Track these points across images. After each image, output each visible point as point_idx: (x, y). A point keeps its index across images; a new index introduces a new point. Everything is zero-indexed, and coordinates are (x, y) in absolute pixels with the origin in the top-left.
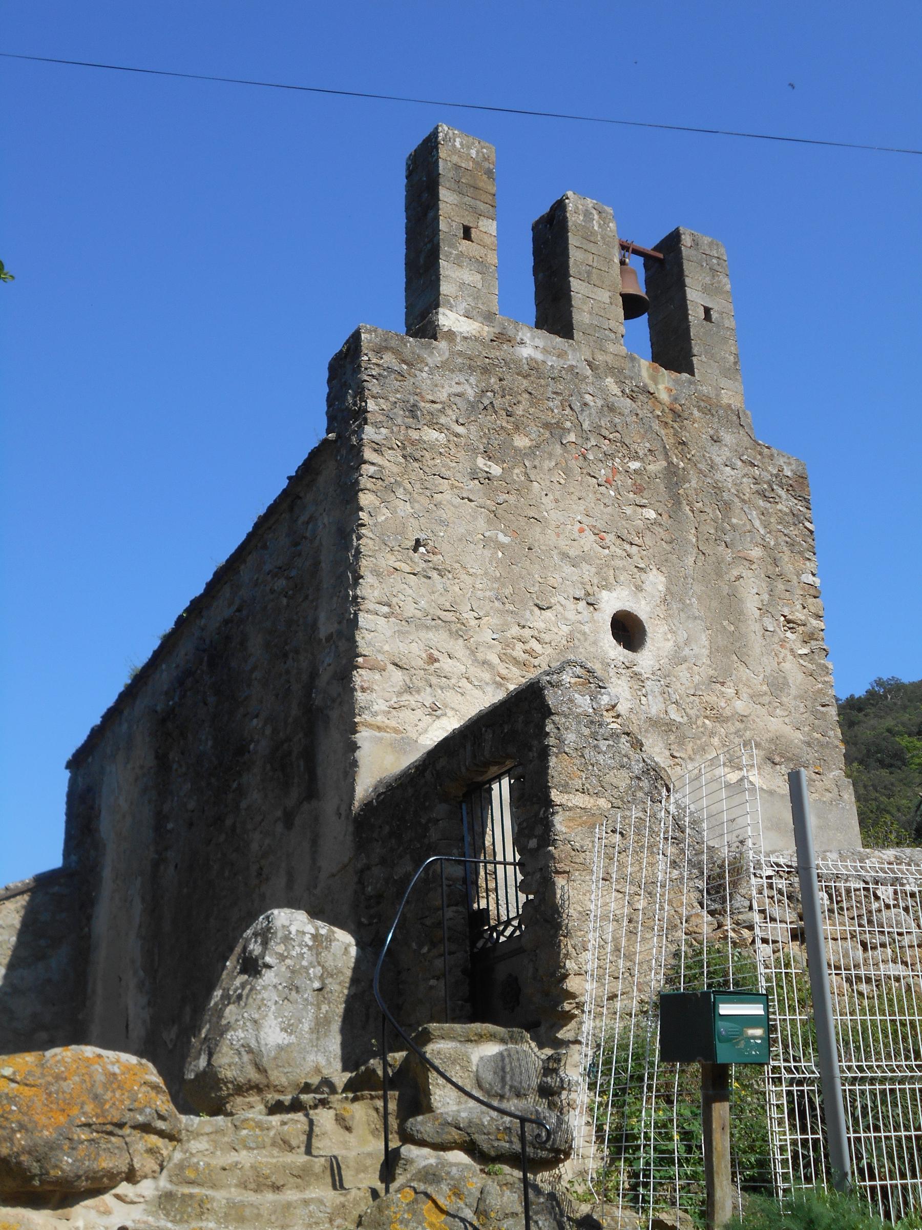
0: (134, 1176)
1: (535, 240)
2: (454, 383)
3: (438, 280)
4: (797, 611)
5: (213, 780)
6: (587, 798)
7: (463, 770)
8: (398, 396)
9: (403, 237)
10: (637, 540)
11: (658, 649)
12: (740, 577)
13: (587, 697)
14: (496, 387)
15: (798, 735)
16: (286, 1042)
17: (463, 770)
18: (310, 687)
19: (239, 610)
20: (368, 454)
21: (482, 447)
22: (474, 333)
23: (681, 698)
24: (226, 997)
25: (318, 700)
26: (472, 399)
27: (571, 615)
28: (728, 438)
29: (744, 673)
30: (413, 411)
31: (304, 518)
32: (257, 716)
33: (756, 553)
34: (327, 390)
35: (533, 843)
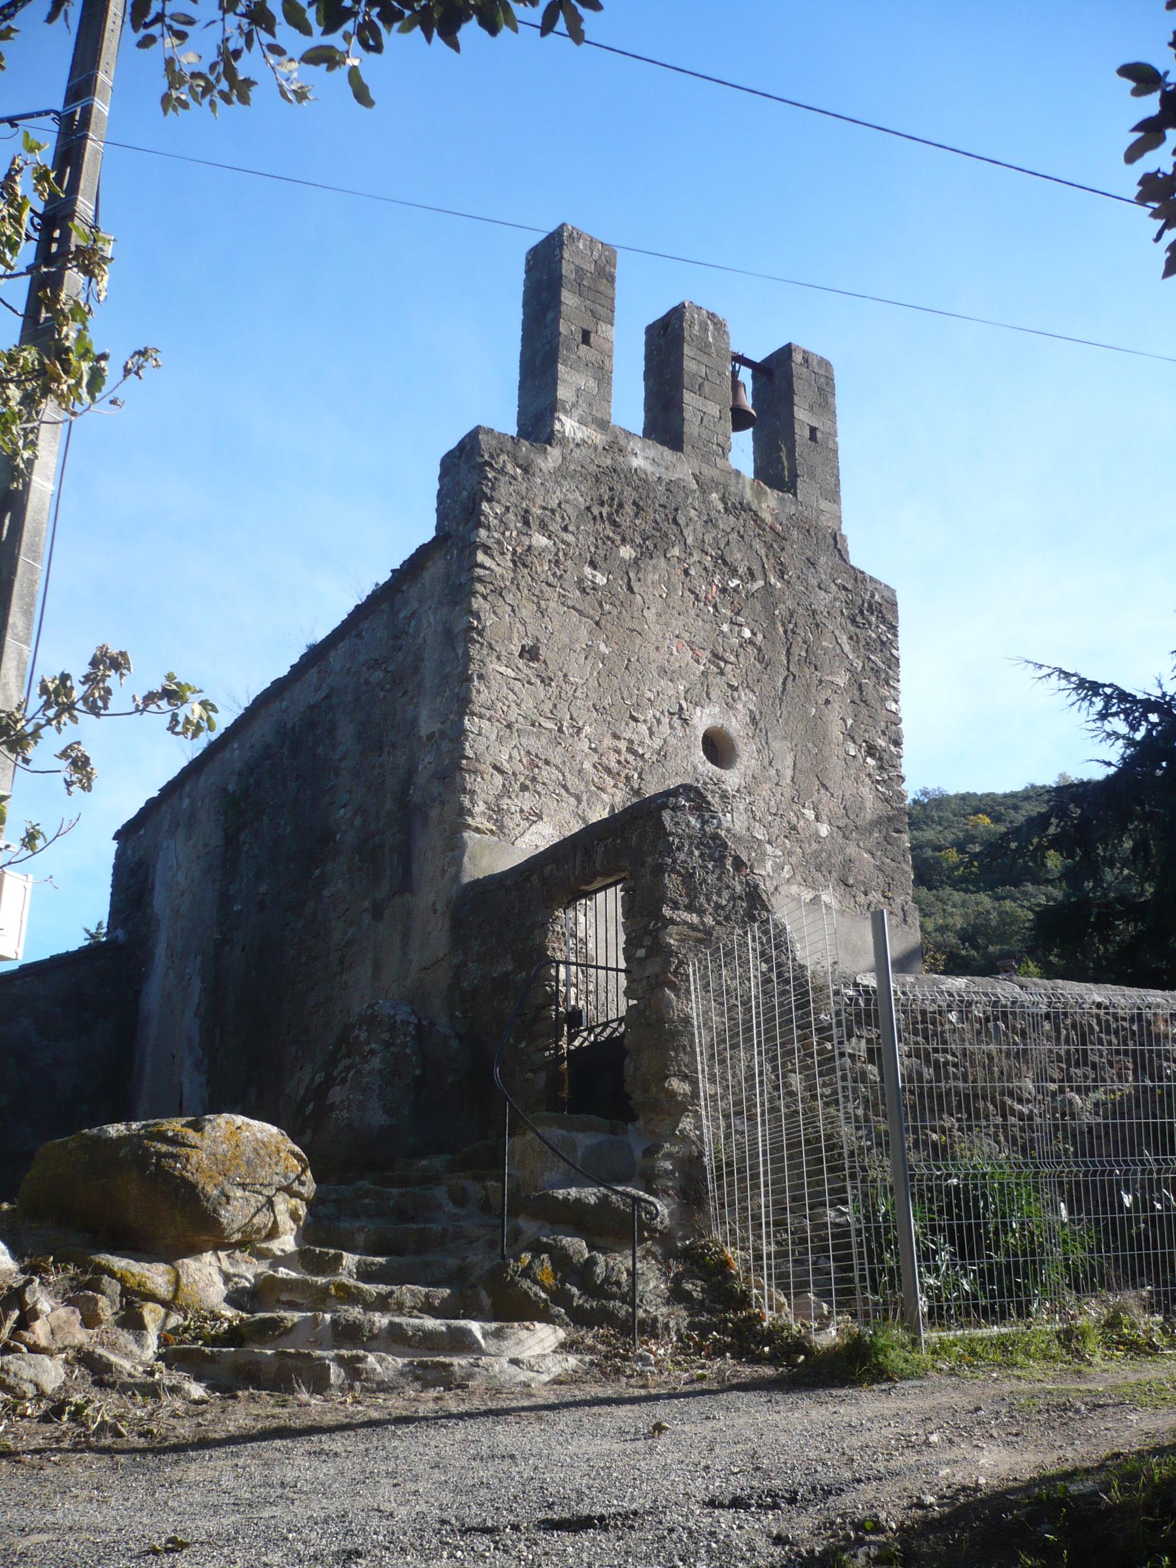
9: (519, 333)
10: (732, 659)
17: (572, 878)
19: (328, 697)
25: (416, 796)
31: (404, 613)
32: (344, 806)
34: (438, 487)
35: (641, 953)
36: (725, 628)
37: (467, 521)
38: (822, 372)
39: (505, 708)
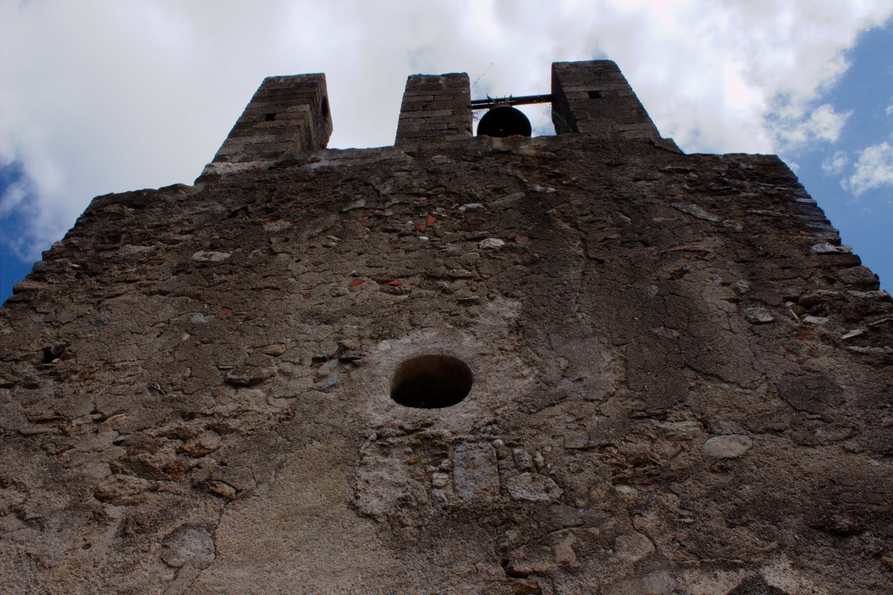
12: (681, 273)
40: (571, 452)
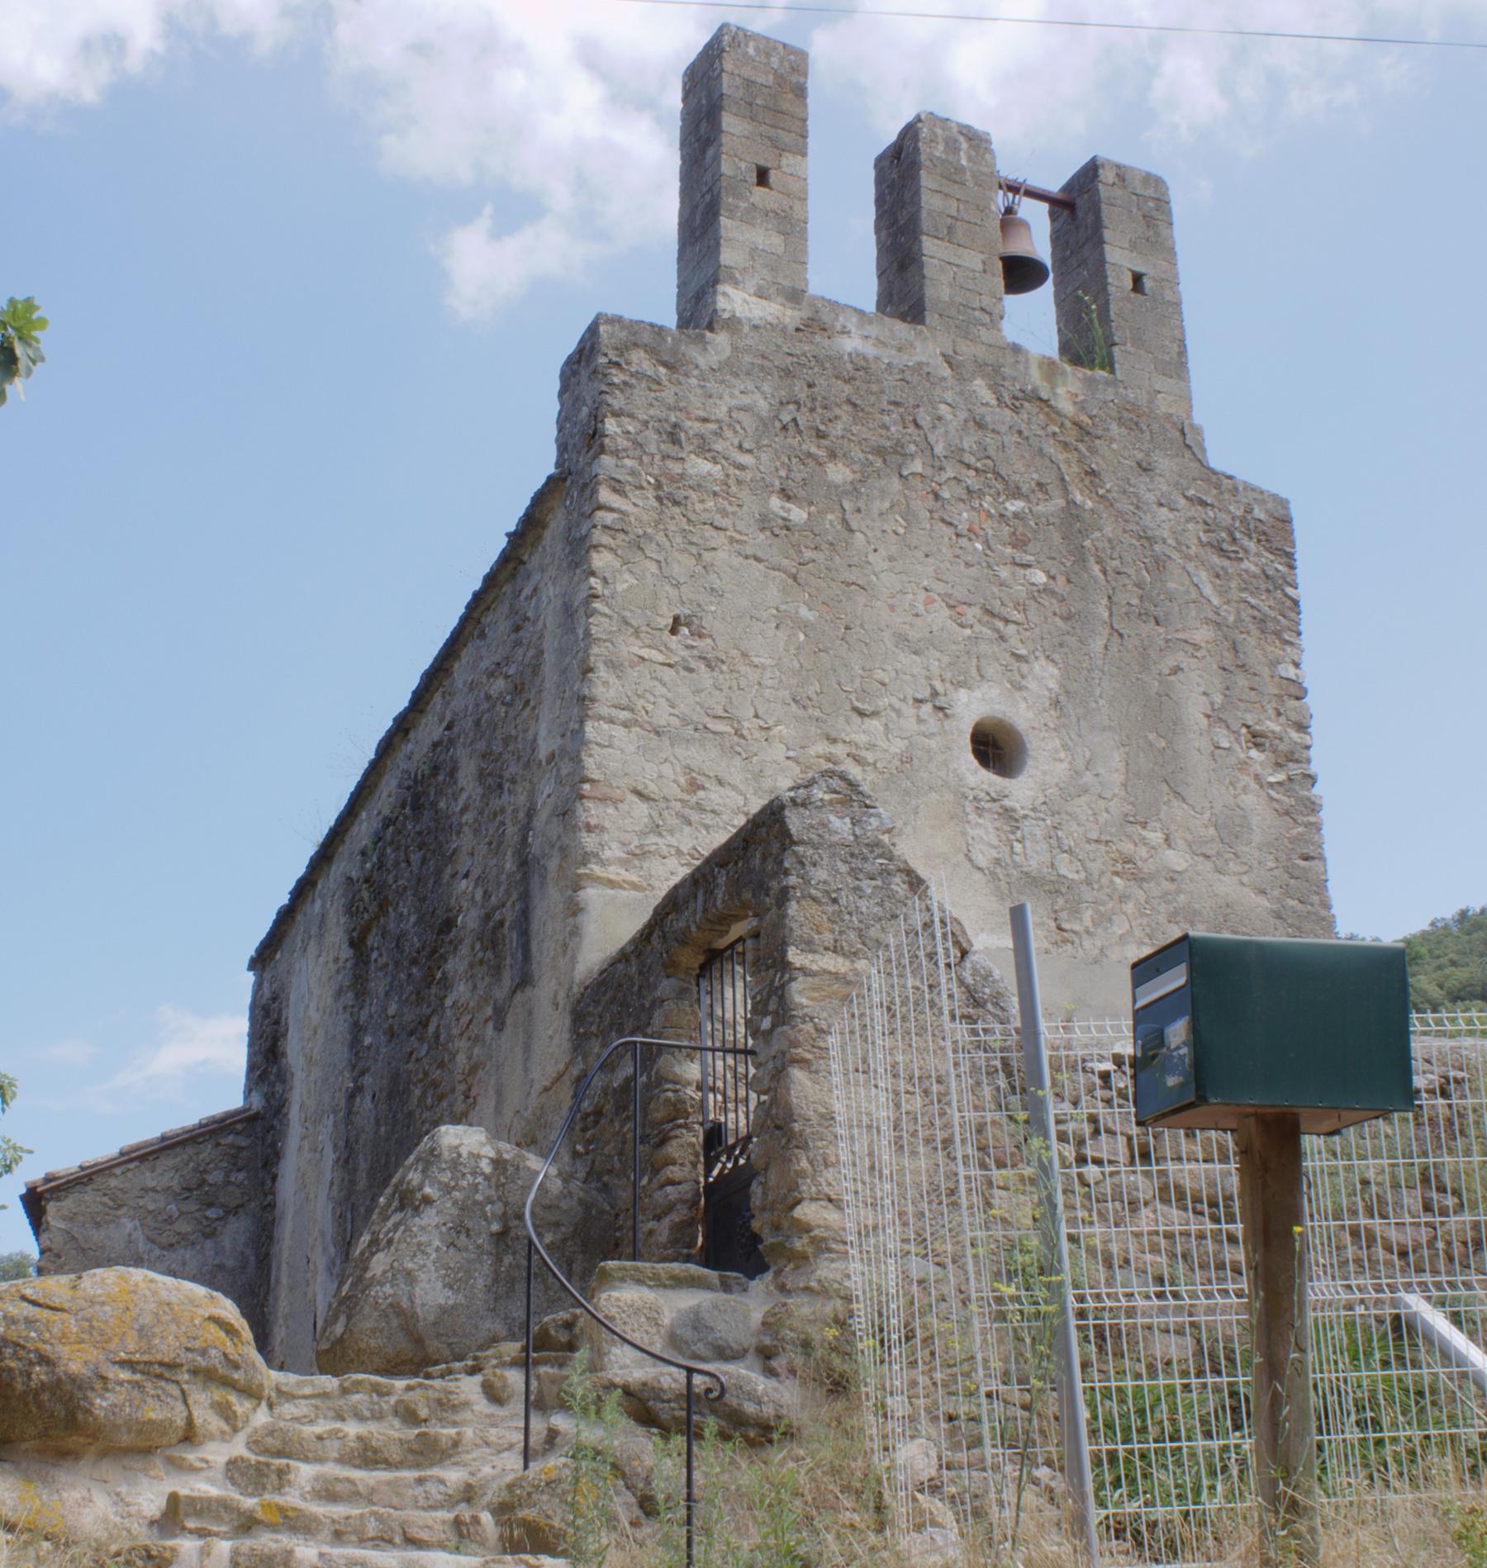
0: (195, 1435)
1: (879, 181)
2: (737, 393)
3: (718, 244)
4: (1269, 719)
5: (415, 970)
6: (840, 960)
7: (693, 929)
8: (651, 412)
11: (1045, 773)
12: (1176, 670)
13: (847, 820)
14: (802, 396)
15: (1264, 902)
16: (451, 1302)
18: (526, 828)
19: (449, 728)
20: (605, 495)
21: (777, 483)
22: (770, 319)
23: (1077, 845)
24: (374, 1242)
25: (536, 844)
26: (764, 414)
27: (910, 724)
28: (1165, 464)
29: (1179, 810)
30: (673, 435)
31: (527, 591)
32: (466, 876)
33: (1203, 634)
34: (558, 407)
35: (766, 1023)
36: (1004, 573)
37: (590, 447)
38: (1150, 192)
39: (650, 708)
40: (1088, 841)
